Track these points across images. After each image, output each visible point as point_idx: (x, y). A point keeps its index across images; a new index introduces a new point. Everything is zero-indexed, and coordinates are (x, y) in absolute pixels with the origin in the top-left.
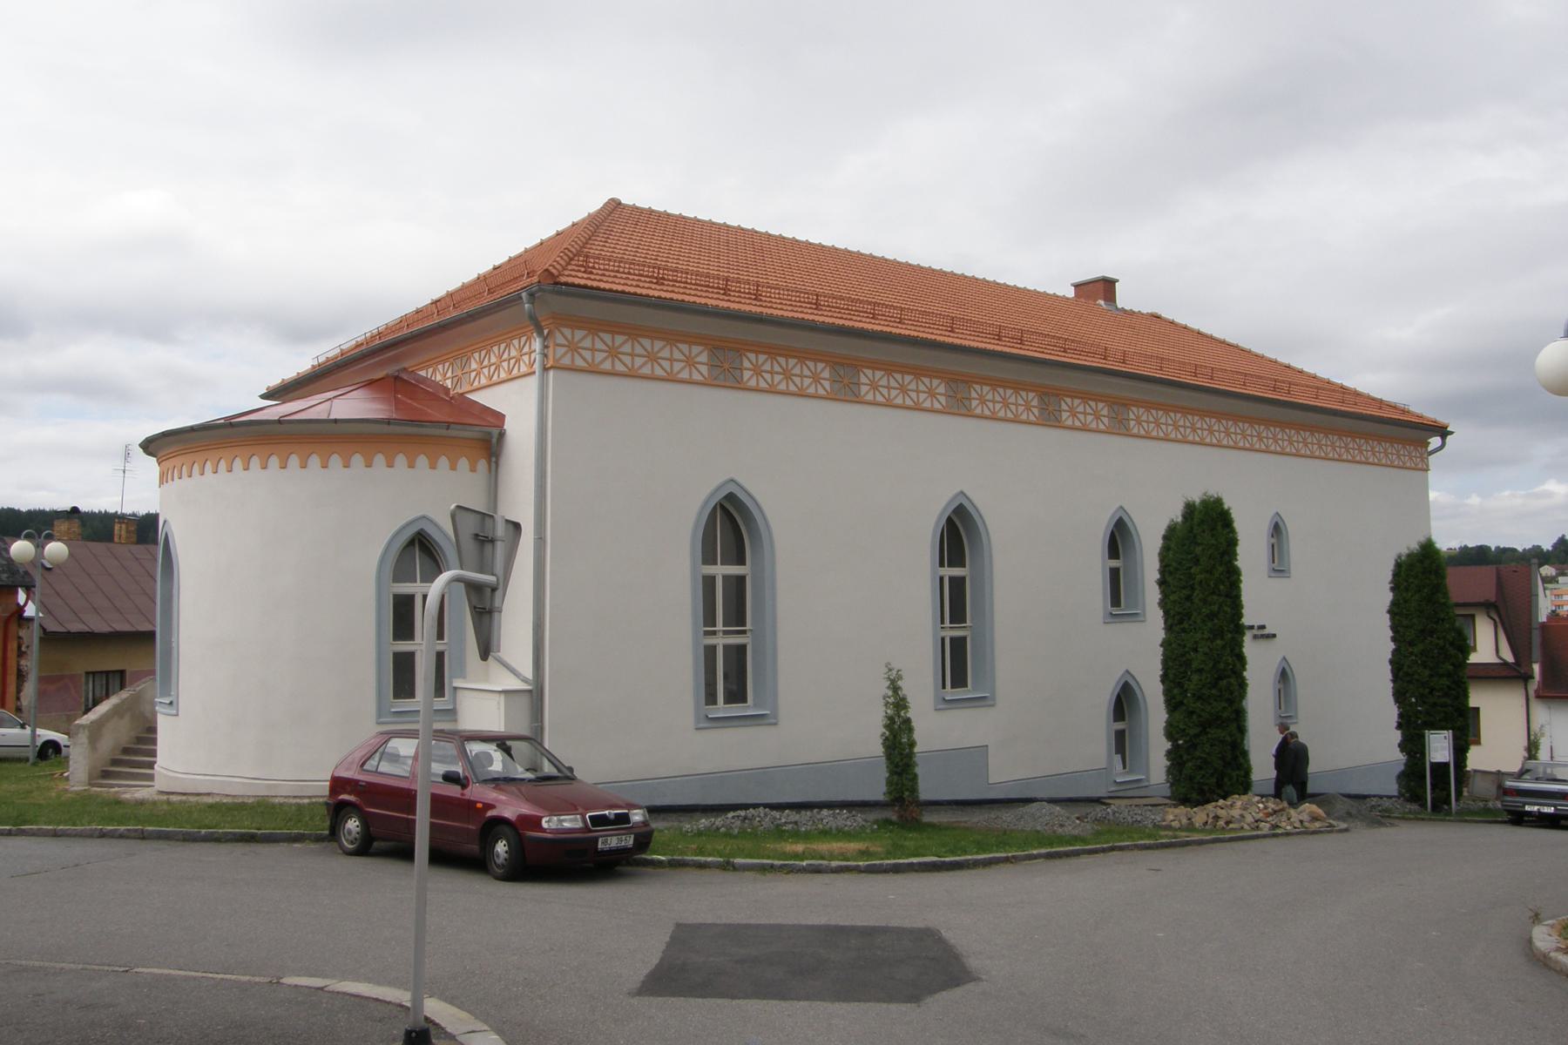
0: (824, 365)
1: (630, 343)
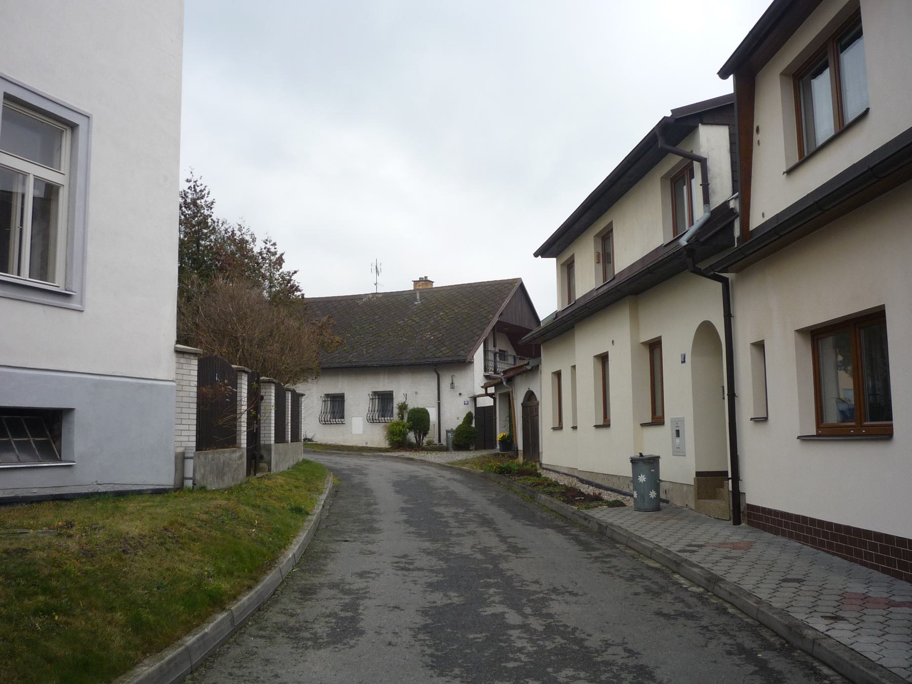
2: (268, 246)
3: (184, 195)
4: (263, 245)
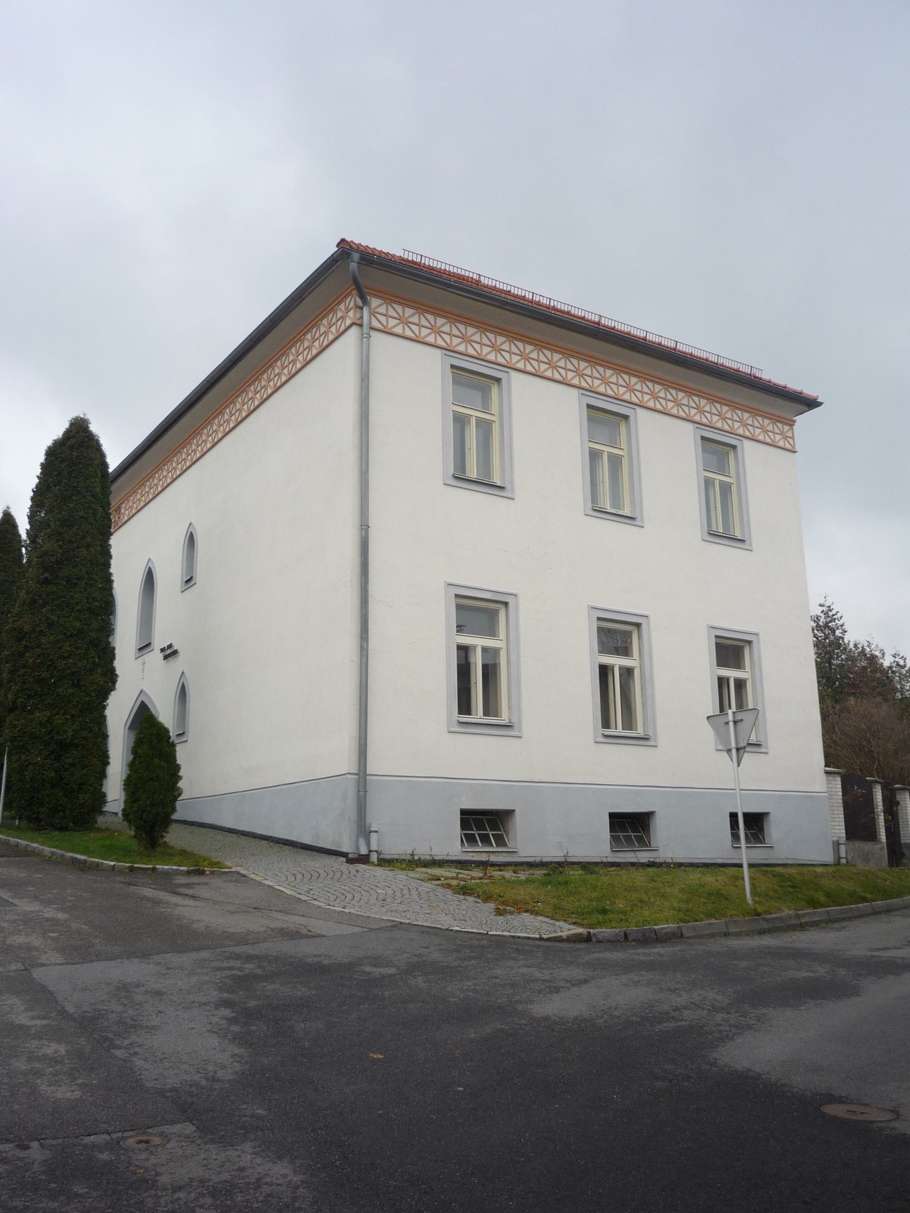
0: (587, 364)
1: (417, 316)
2: (897, 660)
3: (816, 619)
4: (892, 659)
